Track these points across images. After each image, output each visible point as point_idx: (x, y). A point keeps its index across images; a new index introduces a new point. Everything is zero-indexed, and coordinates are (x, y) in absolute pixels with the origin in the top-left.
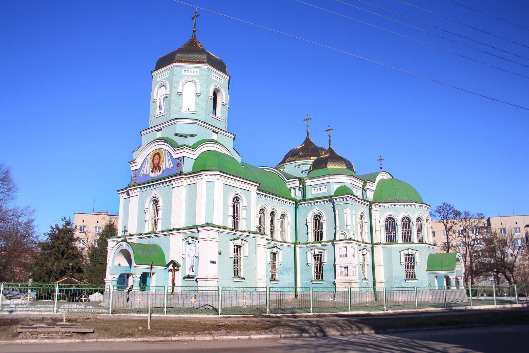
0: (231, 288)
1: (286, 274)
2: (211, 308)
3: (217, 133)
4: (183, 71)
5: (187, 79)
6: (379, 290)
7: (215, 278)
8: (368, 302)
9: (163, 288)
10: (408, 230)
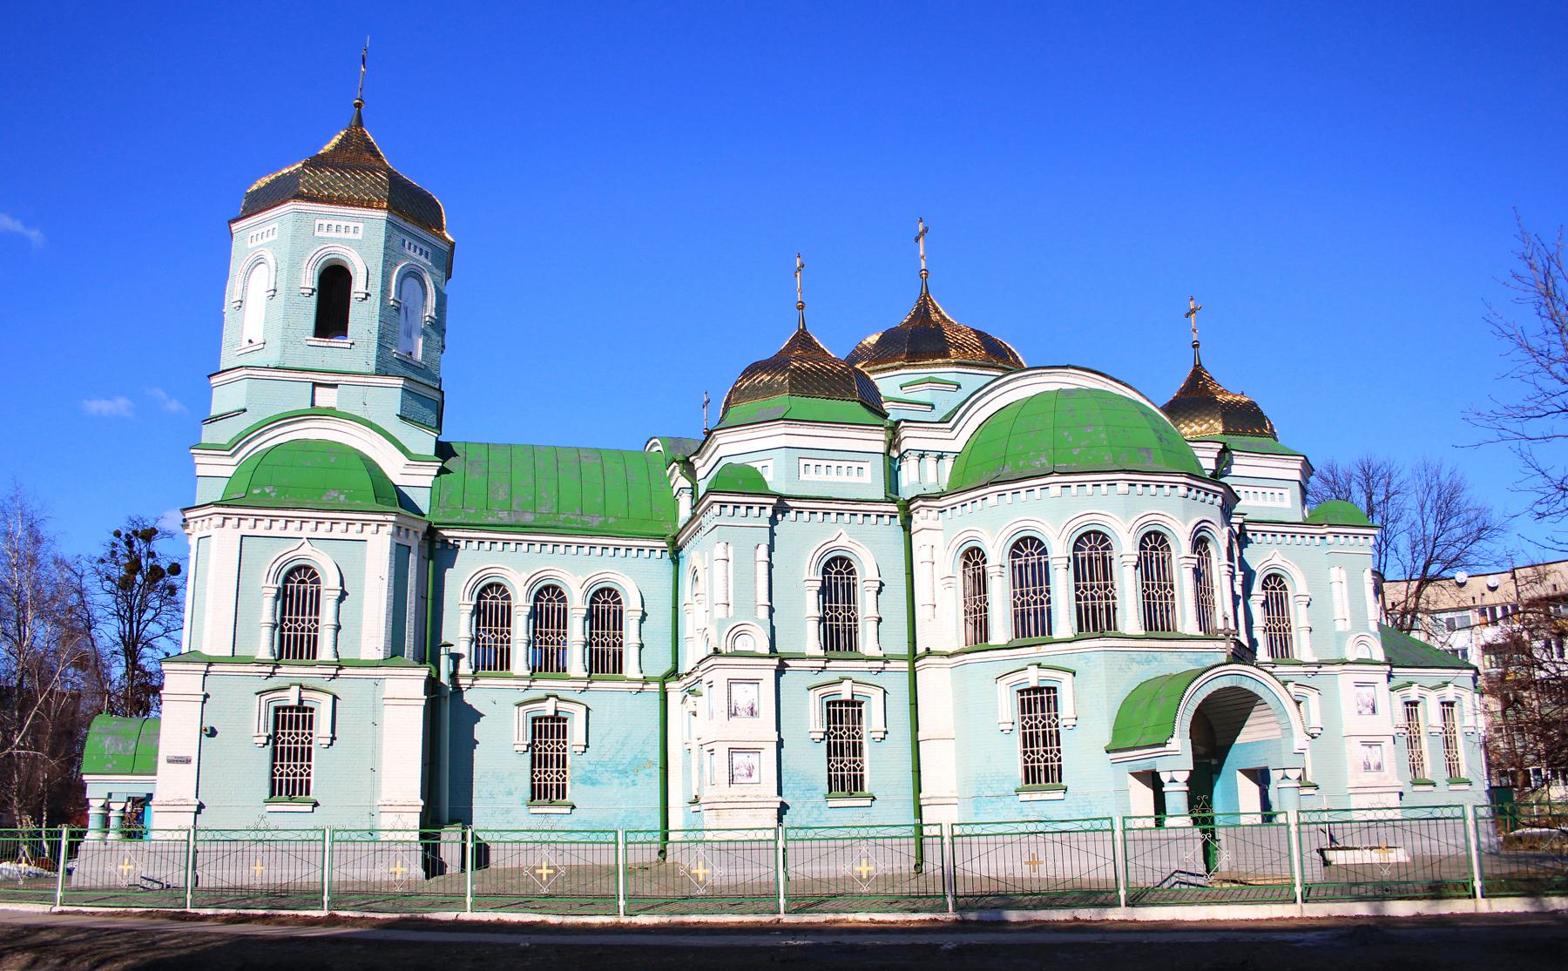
1: (616, 782)
2: (157, 886)
3: (335, 386)
6: (751, 838)
7: (179, 803)
8: (869, 878)
9: (611, 837)
10: (499, 628)
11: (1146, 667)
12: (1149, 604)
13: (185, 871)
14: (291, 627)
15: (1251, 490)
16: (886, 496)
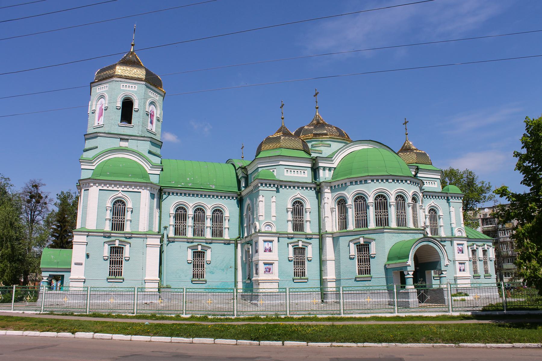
0: (196, 289)
4: (122, 86)
5: (122, 96)
9: (284, 290)
11: (397, 238)
12: (398, 218)
13: (86, 301)
14: (117, 219)
15: (428, 182)
16: (312, 181)
